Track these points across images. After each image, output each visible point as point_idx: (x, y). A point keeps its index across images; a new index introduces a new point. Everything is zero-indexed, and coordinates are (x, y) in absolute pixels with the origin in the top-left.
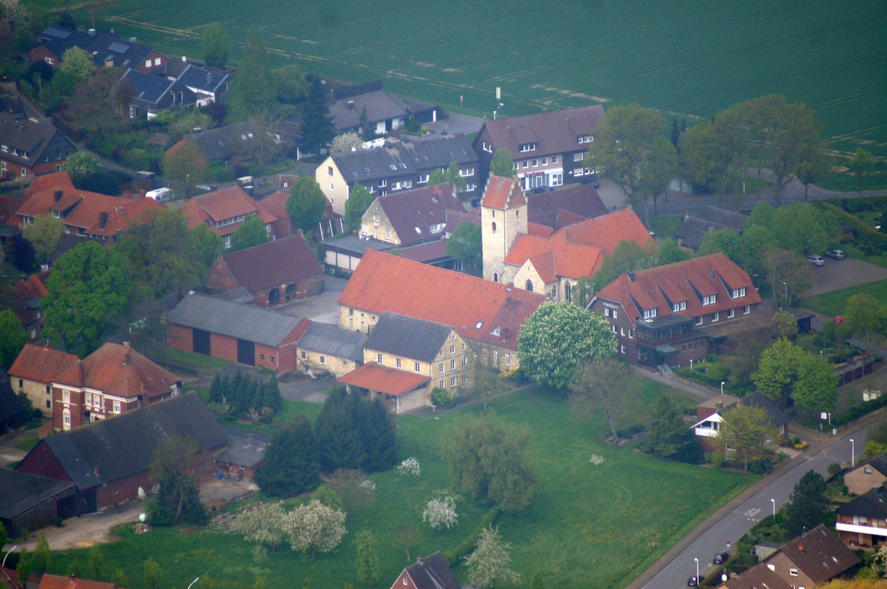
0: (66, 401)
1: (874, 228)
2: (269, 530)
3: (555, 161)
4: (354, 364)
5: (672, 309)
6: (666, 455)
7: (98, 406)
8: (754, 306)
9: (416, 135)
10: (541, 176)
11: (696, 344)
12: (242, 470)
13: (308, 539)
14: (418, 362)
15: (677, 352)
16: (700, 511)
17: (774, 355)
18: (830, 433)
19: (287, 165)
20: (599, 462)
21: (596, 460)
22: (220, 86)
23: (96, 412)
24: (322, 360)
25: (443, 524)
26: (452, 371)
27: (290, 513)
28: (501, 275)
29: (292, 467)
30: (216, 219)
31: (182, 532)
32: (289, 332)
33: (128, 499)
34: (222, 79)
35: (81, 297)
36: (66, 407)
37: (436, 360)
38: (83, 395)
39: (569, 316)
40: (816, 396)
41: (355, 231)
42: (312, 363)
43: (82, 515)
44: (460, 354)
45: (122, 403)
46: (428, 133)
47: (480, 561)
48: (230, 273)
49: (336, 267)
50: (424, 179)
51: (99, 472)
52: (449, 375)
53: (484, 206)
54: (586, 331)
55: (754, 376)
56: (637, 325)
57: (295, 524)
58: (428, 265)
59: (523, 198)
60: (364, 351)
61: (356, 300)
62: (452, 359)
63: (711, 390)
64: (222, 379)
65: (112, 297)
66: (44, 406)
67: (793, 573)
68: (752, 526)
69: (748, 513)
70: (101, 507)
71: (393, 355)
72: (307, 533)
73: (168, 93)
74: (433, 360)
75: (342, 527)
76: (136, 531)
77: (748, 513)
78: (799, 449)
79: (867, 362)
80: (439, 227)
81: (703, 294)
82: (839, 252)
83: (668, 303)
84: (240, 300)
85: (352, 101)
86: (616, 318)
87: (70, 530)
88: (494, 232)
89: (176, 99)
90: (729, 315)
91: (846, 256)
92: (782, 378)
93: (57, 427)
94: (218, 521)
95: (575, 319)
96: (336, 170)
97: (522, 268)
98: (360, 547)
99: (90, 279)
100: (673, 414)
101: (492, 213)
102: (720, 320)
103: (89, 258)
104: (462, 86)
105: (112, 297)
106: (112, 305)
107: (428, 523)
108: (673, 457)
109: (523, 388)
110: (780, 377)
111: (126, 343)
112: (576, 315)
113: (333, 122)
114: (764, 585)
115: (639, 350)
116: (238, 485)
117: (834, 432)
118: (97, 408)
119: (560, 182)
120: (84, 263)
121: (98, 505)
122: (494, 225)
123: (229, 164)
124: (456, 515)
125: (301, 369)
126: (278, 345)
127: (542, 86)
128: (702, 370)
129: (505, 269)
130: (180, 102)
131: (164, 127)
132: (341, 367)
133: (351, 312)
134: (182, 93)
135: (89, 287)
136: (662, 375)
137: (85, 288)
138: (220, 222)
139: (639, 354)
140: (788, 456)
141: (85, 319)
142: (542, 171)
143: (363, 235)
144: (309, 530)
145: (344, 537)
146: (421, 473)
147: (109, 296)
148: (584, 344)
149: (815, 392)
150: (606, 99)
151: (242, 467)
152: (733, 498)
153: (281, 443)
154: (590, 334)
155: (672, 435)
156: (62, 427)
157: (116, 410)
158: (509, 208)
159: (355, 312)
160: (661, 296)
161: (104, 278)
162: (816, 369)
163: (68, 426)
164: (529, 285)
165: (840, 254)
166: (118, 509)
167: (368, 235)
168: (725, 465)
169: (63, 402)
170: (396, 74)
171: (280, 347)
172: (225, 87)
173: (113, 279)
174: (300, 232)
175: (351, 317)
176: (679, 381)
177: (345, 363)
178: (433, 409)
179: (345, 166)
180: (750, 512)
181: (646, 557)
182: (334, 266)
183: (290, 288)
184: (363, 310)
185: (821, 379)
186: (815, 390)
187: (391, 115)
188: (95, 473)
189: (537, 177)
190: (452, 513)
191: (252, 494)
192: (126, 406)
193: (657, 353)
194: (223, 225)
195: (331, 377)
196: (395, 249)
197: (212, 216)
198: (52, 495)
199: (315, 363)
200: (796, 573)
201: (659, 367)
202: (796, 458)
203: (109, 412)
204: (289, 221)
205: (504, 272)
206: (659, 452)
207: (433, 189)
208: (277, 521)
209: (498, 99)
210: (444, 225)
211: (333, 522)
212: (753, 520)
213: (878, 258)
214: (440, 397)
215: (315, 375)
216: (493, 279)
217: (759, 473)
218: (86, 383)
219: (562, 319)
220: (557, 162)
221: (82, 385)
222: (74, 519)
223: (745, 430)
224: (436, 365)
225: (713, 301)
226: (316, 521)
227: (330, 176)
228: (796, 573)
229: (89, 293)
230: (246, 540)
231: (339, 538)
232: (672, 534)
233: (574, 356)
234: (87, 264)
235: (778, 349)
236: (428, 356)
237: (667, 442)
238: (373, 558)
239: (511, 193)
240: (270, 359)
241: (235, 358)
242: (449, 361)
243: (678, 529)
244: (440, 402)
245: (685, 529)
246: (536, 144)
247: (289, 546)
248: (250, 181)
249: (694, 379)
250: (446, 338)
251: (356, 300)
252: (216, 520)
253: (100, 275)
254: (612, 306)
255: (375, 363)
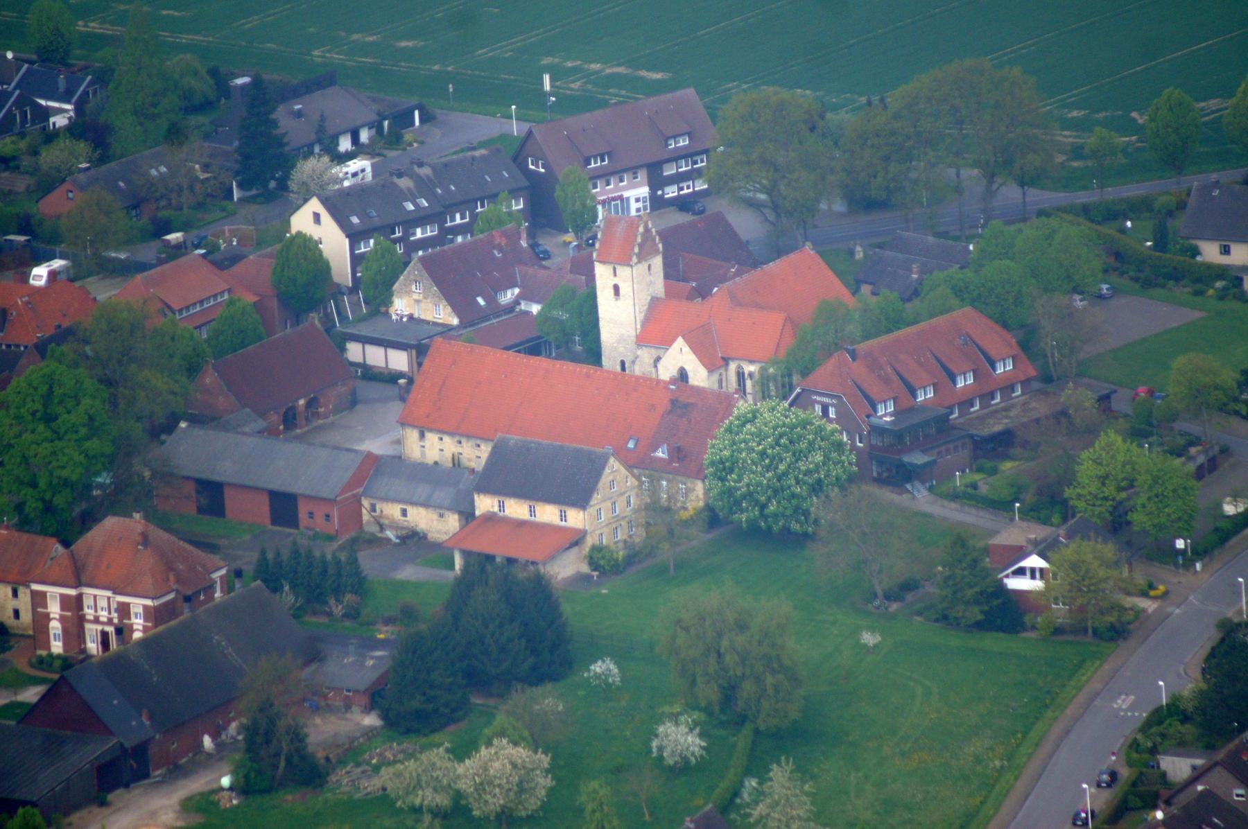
0: (54, 609)
1: (1143, 246)
2: (435, 790)
3: (636, 178)
4: (456, 517)
5: (915, 397)
6: (970, 623)
7: (105, 613)
8: (1025, 383)
9: (397, 149)
10: (619, 202)
11: (956, 448)
12: (347, 697)
13: (499, 799)
14: (564, 508)
15: (934, 462)
16: (1047, 706)
17: (1098, 458)
18: (1192, 569)
19: (223, 210)
20: (875, 641)
21: (869, 639)
22: (80, 97)
23: (103, 623)
24: (404, 513)
25: (685, 760)
26: (614, 518)
27: (467, 761)
28: (633, 362)
29: (432, 687)
30: (176, 307)
31: (290, 800)
32: (349, 474)
33: (190, 755)
34: (83, 82)
35: (46, 448)
36: (137, 630)
37: (592, 503)
38: (79, 598)
39: (784, 423)
40: (1169, 515)
41: (383, 309)
42: (388, 518)
43: (132, 786)
44: (623, 490)
45: (145, 607)
46: (415, 145)
47: (772, 814)
48: (225, 388)
49: (364, 366)
50: (453, 219)
51: (150, 718)
52: (610, 524)
53: (600, 262)
54: (811, 443)
55: (1068, 492)
56: (870, 426)
57: (476, 778)
58: (510, 352)
59: (656, 245)
60: (476, 497)
61: (428, 416)
62: (613, 500)
63: (996, 516)
64: (270, 556)
65: (93, 445)
66: (10, 617)
67: (1238, 796)
68: (1138, 725)
69: (1117, 703)
70: (157, 768)
71: (523, 501)
72: (497, 790)
73: (10, 110)
74: (587, 504)
75: (546, 777)
76: (221, 803)
77: (1117, 703)
78: (1155, 598)
79: (1211, 454)
80: (509, 293)
81: (955, 371)
82: (1105, 287)
83: (906, 386)
84: (247, 429)
85: (300, 106)
86: (834, 417)
87: (119, 810)
88: (617, 299)
89: (21, 121)
90: (993, 399)
91: (1115, 291)
92: (1114, 493)
93: (40, 648)
94: (343, 781)
95: (793, 427)
96: (326, 217)
97: (670, 350)
98: (590, 807)
99: (56, 419)
100: (975, 562)
101: (612, 270)
102: (982, 407)
103: (51, 387)
104: (436, 67)
105: (93, 445)
106: (94, 457)
107: (661, 758)
108: (979, 626)
109: (716, 533)
110: (1109, 491)
111: (137, 516)
112: (794, 420)
113: (285, 140)
114: (1216, 821)
115: (874, 462)
116: (346, 719)
117: (1198, 566)
118: (90, 614)
119: (645, 207)
120: (42, 396)
121: (151, 768)
122: (616, 289)
123: (137, 216)
124: (703, 744)
125: (374, 529)
126: (336, 497)
127: (556, 60)
128: (974, 486)
129: (639, 352)
130: (27, 123)
131: (12, 164)
132: (435, 522)
133: (422, 436)
134: (28, 109)
135: (55, 432)
136: (914, 498)
137: (49, 434)
138: (180, 311)
139: (874, 468)
140: (1144, 610)
141: (55, 481)
142: (619, 194)
143: (397, 314)
144: (499, 786)
145: (551, 792)
146: (622, 681)
147: (87, 444)
148: (811, 463)
149: (1166, 510)
150: (662, 74)
151: (348, 691)
152: (1087, 681)
153: (414, 652)
154: (817, 446)
155: (976, 593)
156: (48, 647)
157: (136, 618)
158: (639, 262)
159: (429, 435)
160: (895, 378)
161: (77, 417)
162: (1165, 474)
163: (57, 646)
164: (683, 375)
165: (1107, 289)
166: (177, 771)
167: (406, 313)
168: (1058, 631)
169: (49, 610)
170: (327, 55)
171: (338, 499)
172: (88, 93)
173: (91, 419)
174: (313, 318)
175: (422, 444)
176: (943, 506)
177: (441, 516)
178: (593, 576)
179: (339, 206)
180: (1119, 701)
181: (994, 786)
182: (360, 363)
183: (310, 404)
184: (442, 431)
185: (1174, 491)
186: (1166, 506)
187: (358, 123)
188: (144, 719)
189: (613, 203)
190: (698, 741)
191: (375, 732)
192: (153, 610)
193: (901, 465)
194: (185, 314)
195: (420, 538)
196: (453, 333)
197: (168, 301)
198: (89, 760)
199: (393, 519)
200: (1242, 796)
201: (909, 486)
202: (1155, 611)
203: (125, 621)
204: (275, 299)
205: (637, 357)
206: (956, 618)
207: (493, 236)
208: (444, 775)
209: (546, 92)
210: (517, 291)
211: (533, 770)
212: (1129, 714)
213: (1161, 291)
214: (603, 558)
215: (397, 537)
216: (619, 368)
217: (1112, 639)
218: (83, 580)
219: (775, 428)
220: (639, 179)
221: (78, 584)
222: (120, 792)
223: (1091, 578)
224: (591, 510)
225: (970, 381)
226: (509, 772)
227: (317, 226)
228: (1242, 796)
229: (56, 442)
230: (400, 807)
231: (543, 793)
232: (1018, 746)
233: (798, 482)
234: (48, 397)
235: (1103, 449)
236: (582, 502)
237: (967, 603)
238: (610, 822)
239: (639, 240)
240: (324, 517)
241: (267, 521)
242: (609, 504)
243: (1024, 737)
244: (603, 567)
245: (1032, 734)
246: (609, 154)
247: (467, 811)
248: (182, 239)
249: (965, 501)
250: (603, 468)
251: (428, 416)
252: (338, 778)
253: (69, 412)
254: (826, 400)
255: (494, 514)
